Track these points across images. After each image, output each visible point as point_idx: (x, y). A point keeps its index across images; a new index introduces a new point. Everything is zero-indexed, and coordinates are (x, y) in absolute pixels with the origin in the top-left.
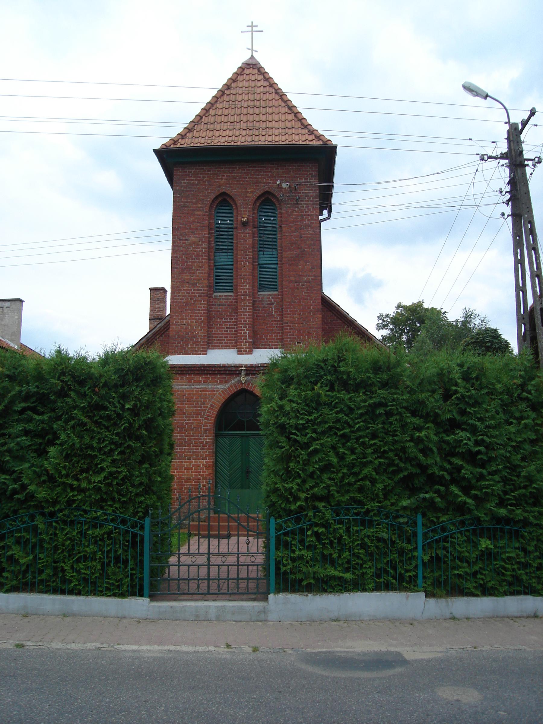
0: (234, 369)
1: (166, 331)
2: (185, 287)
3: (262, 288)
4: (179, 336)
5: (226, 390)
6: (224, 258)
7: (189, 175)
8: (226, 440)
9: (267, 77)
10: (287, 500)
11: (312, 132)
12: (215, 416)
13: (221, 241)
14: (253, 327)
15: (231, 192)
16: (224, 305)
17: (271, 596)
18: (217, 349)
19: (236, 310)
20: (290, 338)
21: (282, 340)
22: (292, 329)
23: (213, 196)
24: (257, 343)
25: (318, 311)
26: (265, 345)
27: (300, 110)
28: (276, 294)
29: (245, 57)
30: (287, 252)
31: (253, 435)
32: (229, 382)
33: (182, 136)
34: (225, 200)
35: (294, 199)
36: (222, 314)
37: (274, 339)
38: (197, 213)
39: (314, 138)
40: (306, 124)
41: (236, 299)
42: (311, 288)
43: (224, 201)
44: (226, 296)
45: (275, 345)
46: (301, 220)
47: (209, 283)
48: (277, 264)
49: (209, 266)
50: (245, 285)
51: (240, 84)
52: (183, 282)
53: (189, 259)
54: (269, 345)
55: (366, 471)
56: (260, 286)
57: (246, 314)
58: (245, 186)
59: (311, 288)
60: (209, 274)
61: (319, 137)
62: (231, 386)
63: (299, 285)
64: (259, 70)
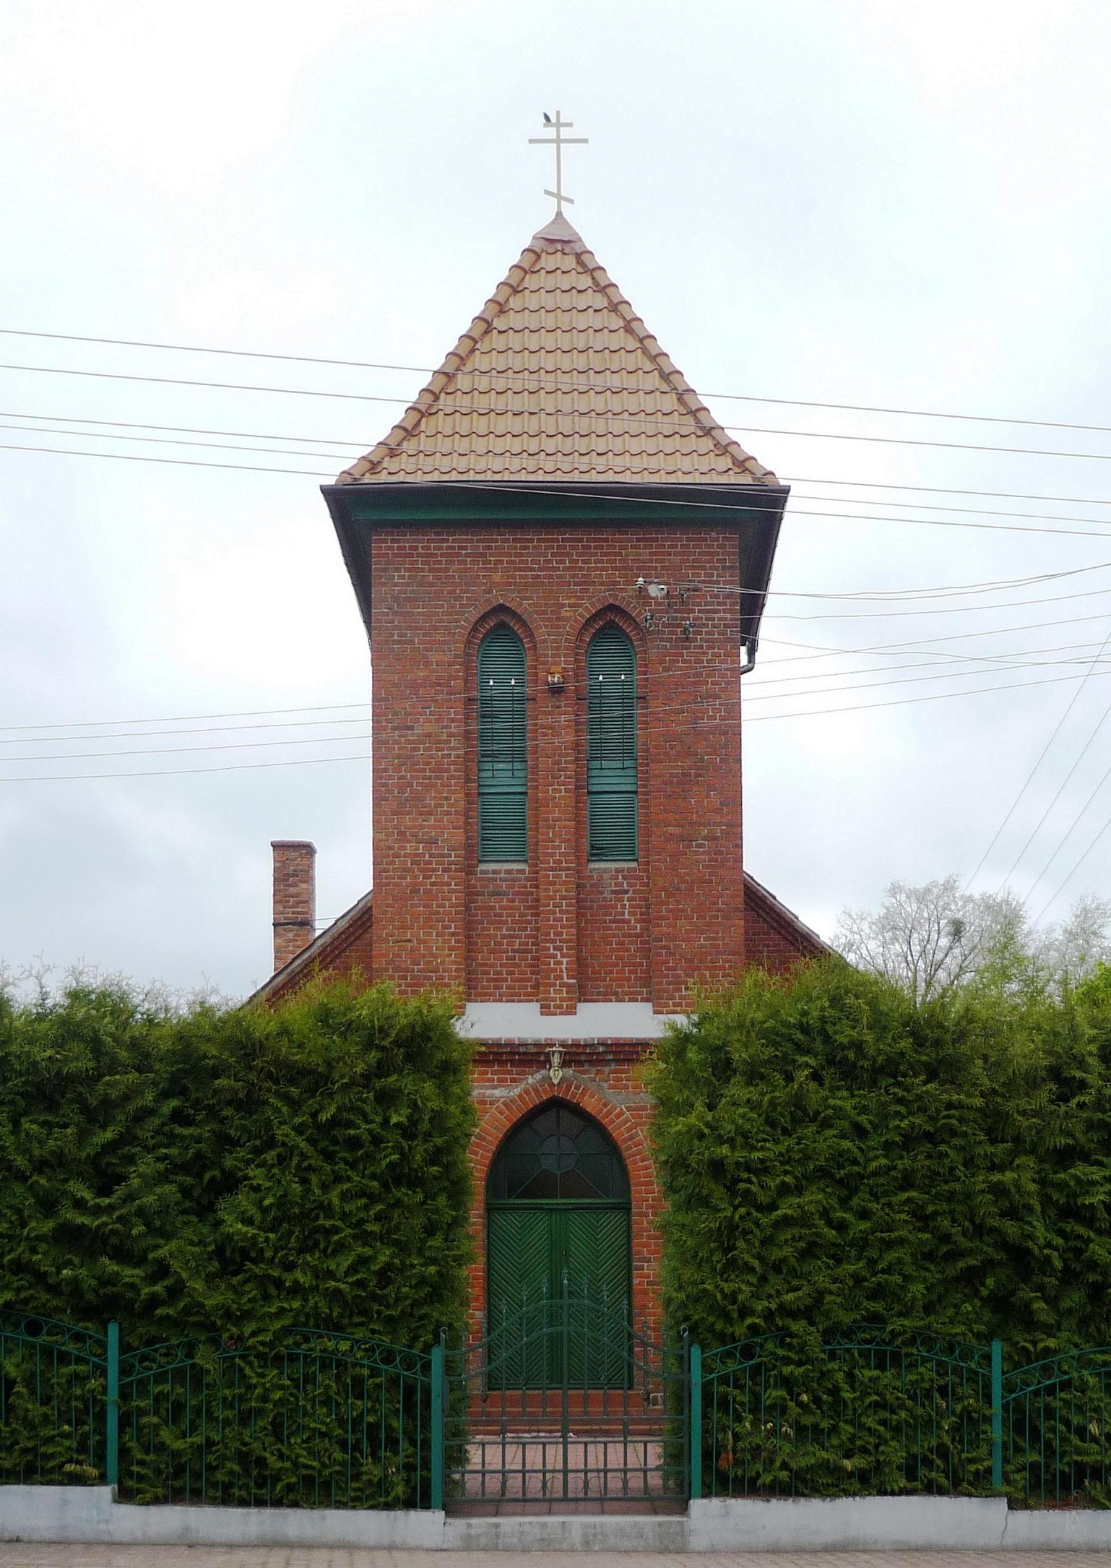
0: (534, 1050)
1: (338, 956)
2: (409, 848)
3: (598, 852)
4: (396, 969)
5: (513, 1101)
6: (503, 776)
7: (411, 555)
8: (514, 1219)
9: (603, 284)
10: (726, 1316)
11: (725, 448)
12: (487, 1162)
13: (493, 731)
14: (578, 948)
15: (523, 604)
16: (505, 894)
17: (697, 1505)
18: (488, 1001)
19: (535, 906)
20: (668, 976)
21: (646, 981)
22: (674, 954)
23: (473, 614)
24: (587, 987)
25: (738, 910)
26: (606, 994)
27: (706, 402)
28: (633, 870)
29: (538, 220)
30: (660, 761)
31: (577, 1208)
32: (520, 1080)
33: (390, 449)
34: (502, 625)
35: (679, 626)
36: (500, 915)
37: (629, 979)
38: (434, 657)
39: (731, 466)
40: (708, 425)
41: (535, 881)
42: (720, 853)
43: (501, 628)
44: (508, 872)
45: (629, 993)
46: (694, 683)
47: (468, 838)
48: (635, 792)
49: (467, 795)
50: (558, 850)
51: (533, 301)
52: (402, 833)
53: (417, 778)
54: (616, 994)
55: (892, 1256)
56: (593, 848)
57: (559, 914)
58: (556, 587)
59: (720, 853)
60: (467, 817)
61: (743, 463)
62: (526, 1091)
63: (689, 846)
64: (580, 262)
